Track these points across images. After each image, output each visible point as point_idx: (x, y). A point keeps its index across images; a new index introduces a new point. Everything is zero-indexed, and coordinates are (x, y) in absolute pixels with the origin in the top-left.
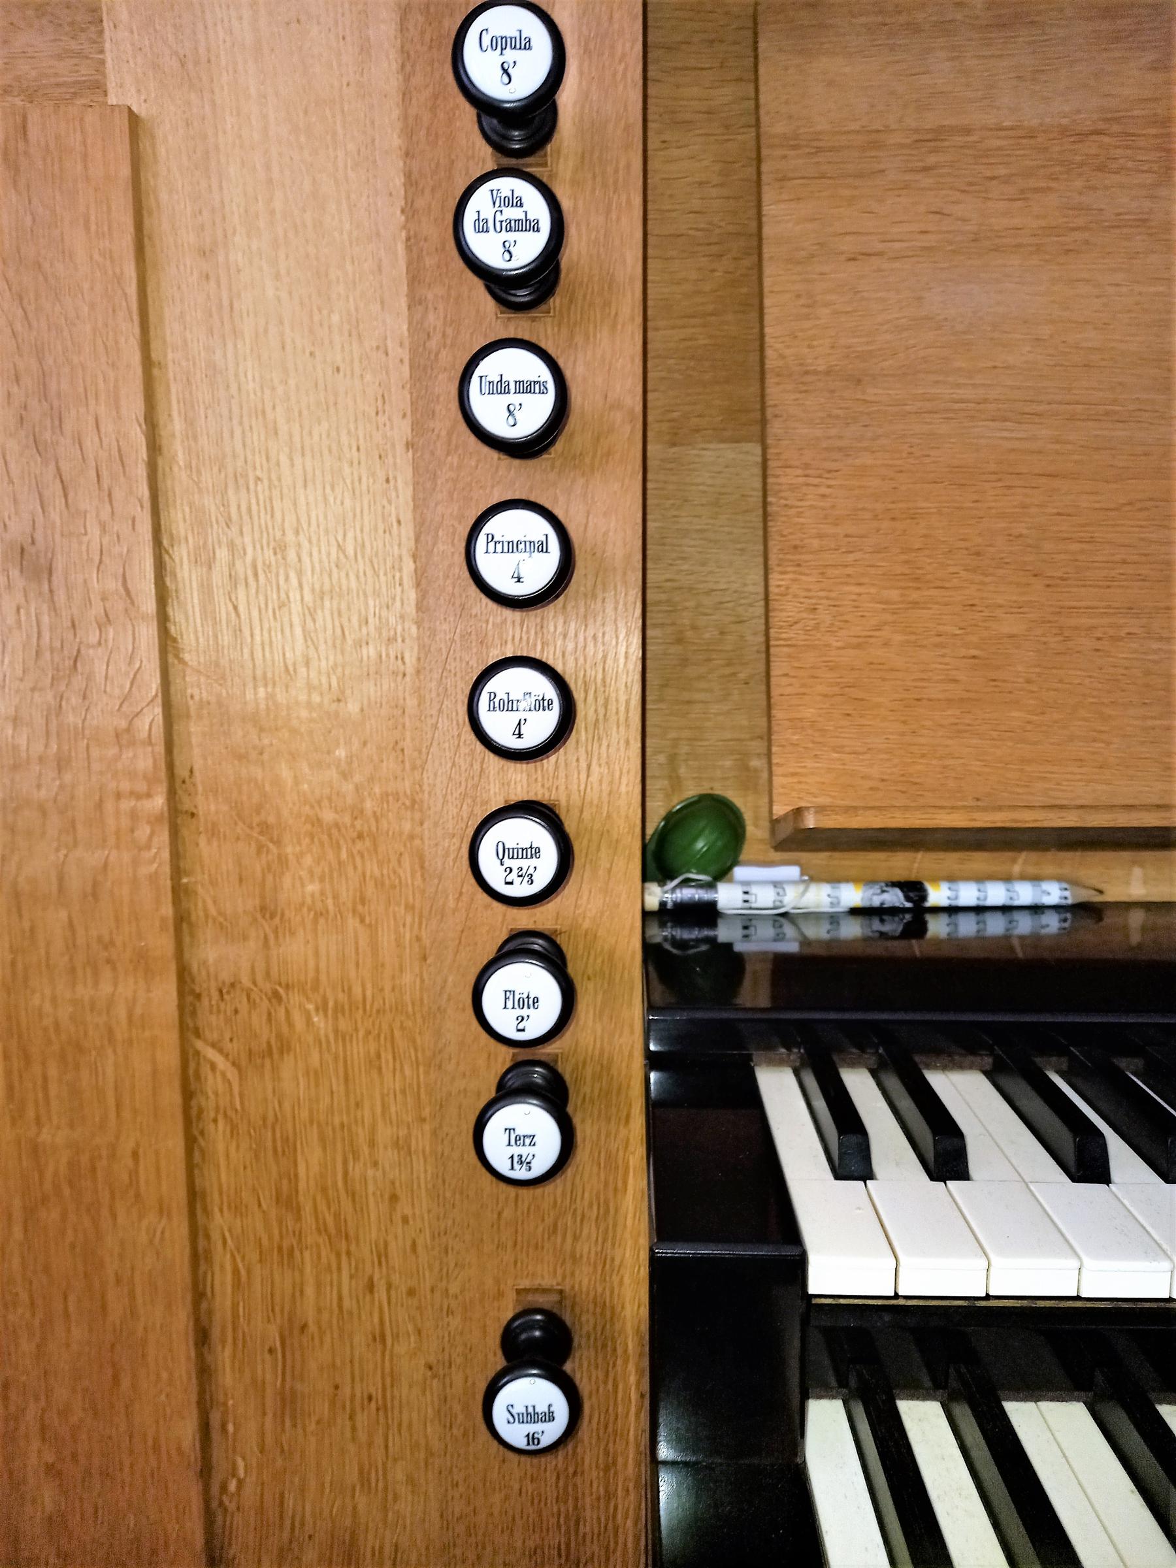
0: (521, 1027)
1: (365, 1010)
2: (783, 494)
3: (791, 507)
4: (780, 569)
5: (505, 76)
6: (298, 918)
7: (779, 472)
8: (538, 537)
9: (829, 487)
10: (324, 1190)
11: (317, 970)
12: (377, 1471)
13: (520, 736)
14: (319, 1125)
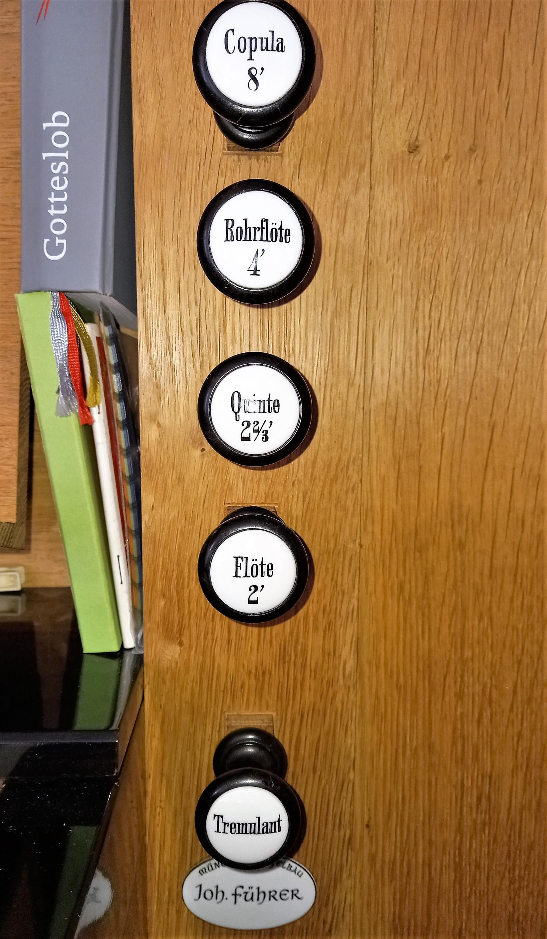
0: (253, 598)
5: (252, 83)
12: (515, 834)
13: (255, 272)
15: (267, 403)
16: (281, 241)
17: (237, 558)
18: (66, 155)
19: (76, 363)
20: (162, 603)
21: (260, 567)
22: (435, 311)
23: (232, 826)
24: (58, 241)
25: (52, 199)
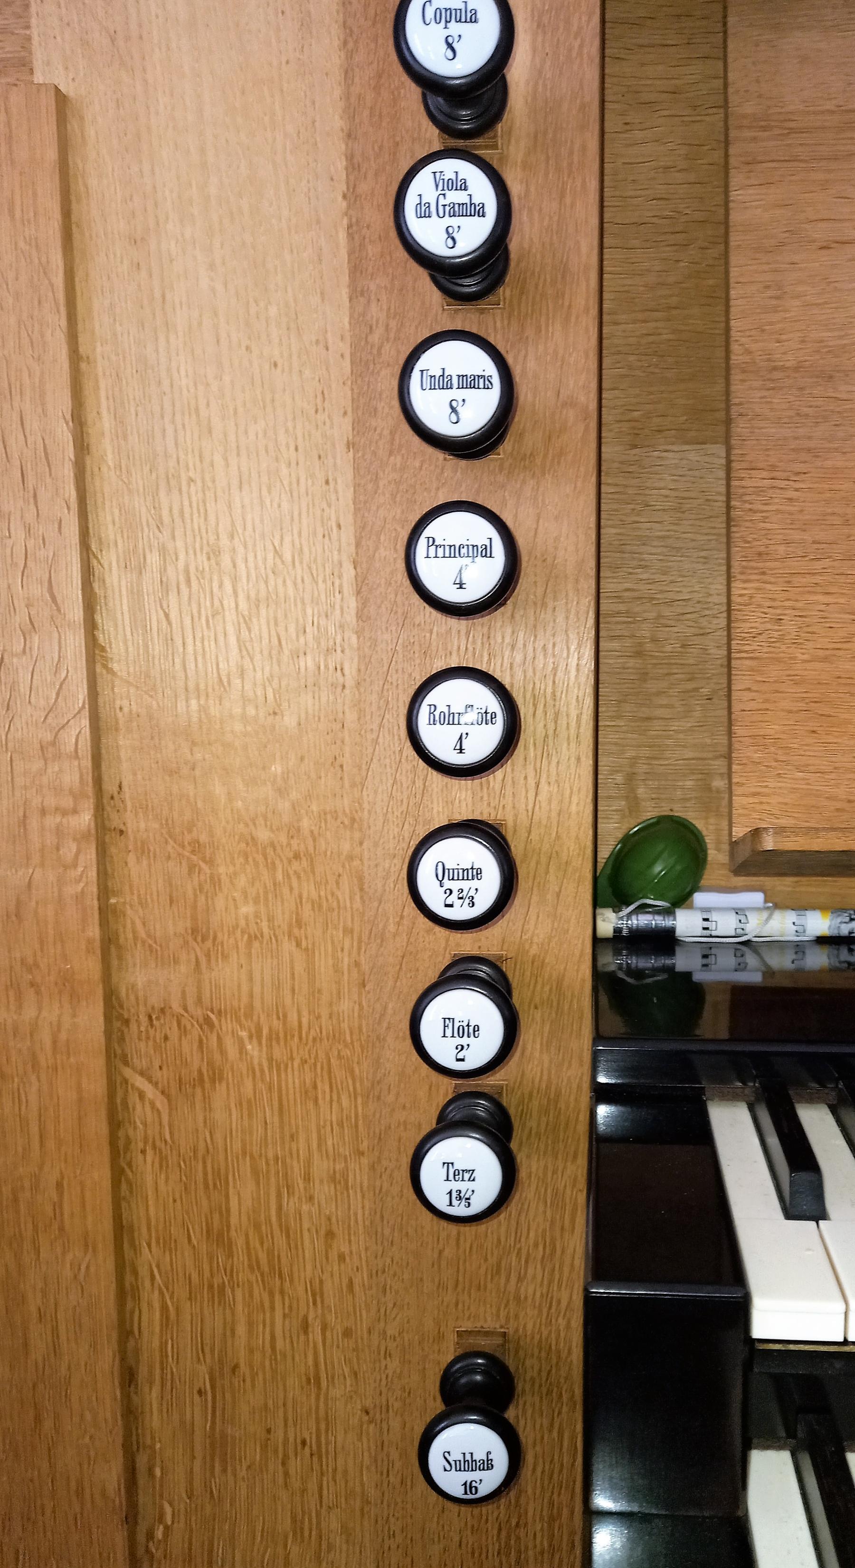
0: (460, 1056)
1: (300, 1038)
2: (747, 498)
3: (755, 512)
4: (743, 577)
6: (232, 941)
7: (743, 474)
8: (482, 541)
9: (797, 490)
10: (257, 1226)
11: (251, 996)
14: (252, 1157)
15: (470, 871)
16: (469, 1037)
17: (445, 1019)
21: (466, 1028)
22: (698, 780)
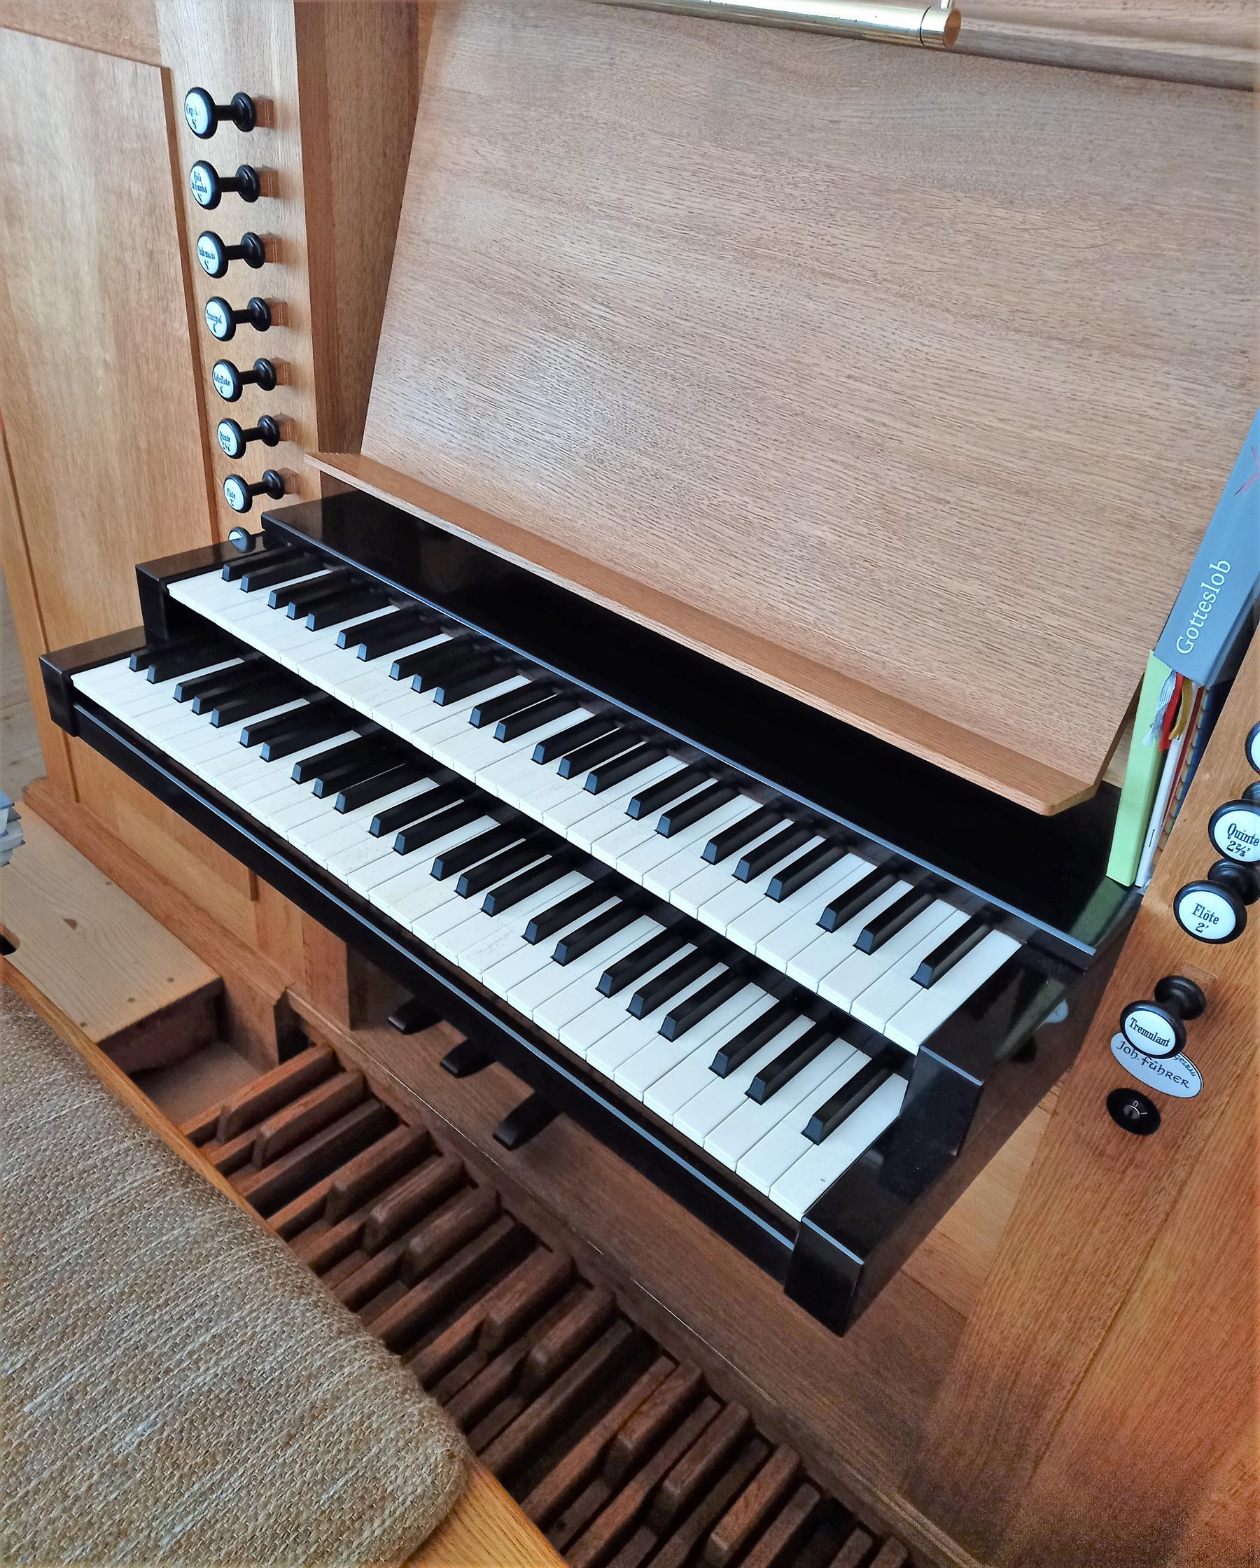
18: (1218, 591)
19: (1172, 714)
20: (1168, 877)
23: (1140, 1028)
24: (1188, 642)
25: (1196, 615)
